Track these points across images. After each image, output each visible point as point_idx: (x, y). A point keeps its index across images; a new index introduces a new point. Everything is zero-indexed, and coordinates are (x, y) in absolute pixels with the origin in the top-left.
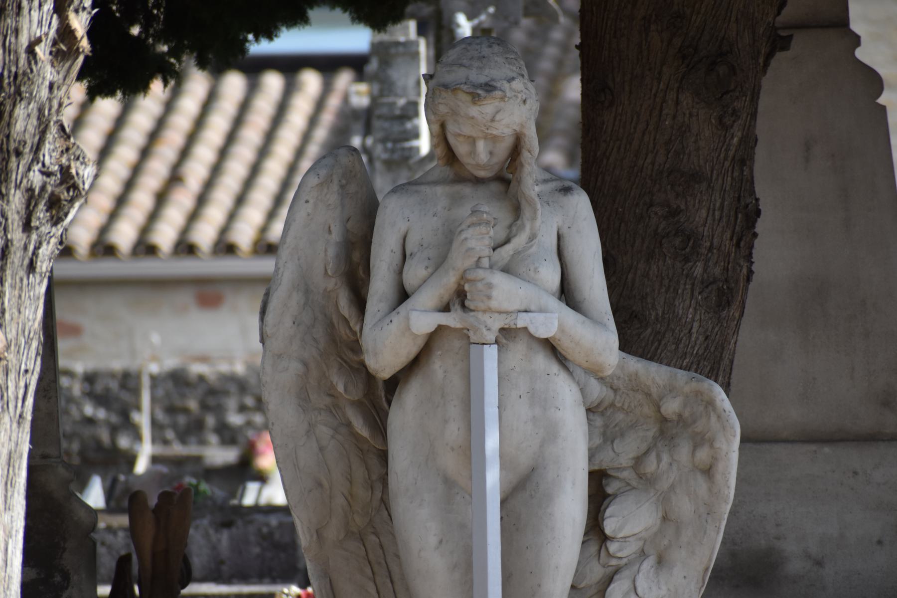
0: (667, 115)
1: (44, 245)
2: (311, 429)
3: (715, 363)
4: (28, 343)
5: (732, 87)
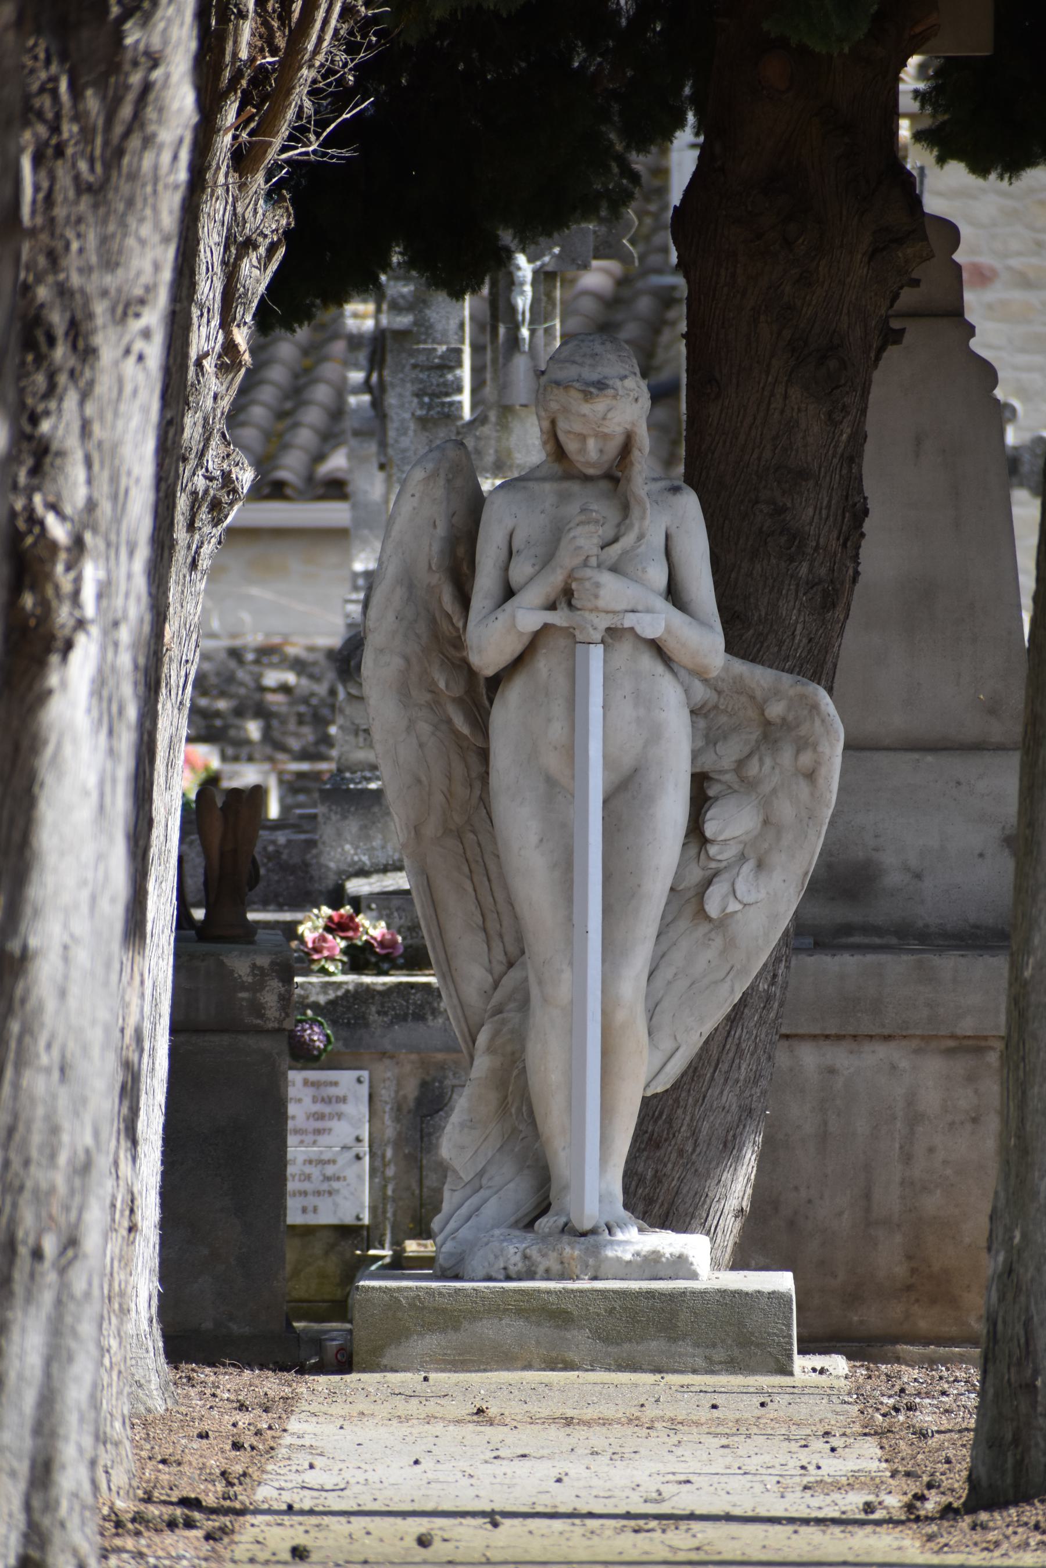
0: (775, 409)
1: (206, 546)
2: (411, 724)
3: (818, 665)
4: (189, 635)
5: (843, 381)
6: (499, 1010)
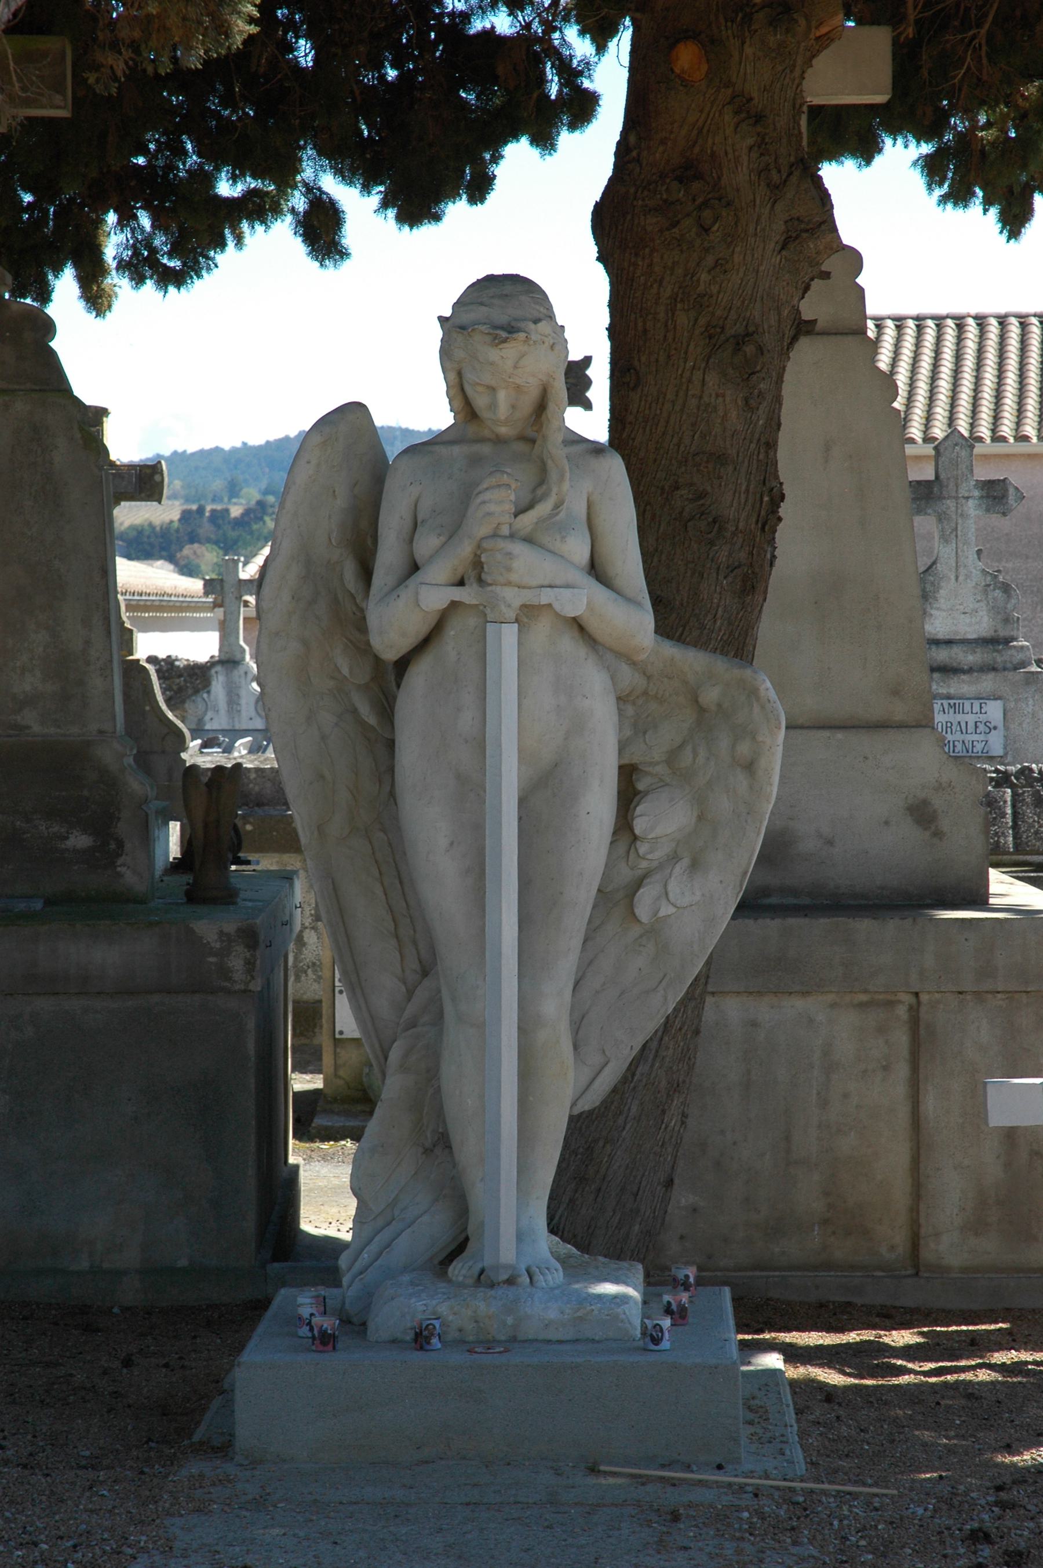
5: (758, 368)
6: (412, 1024)
